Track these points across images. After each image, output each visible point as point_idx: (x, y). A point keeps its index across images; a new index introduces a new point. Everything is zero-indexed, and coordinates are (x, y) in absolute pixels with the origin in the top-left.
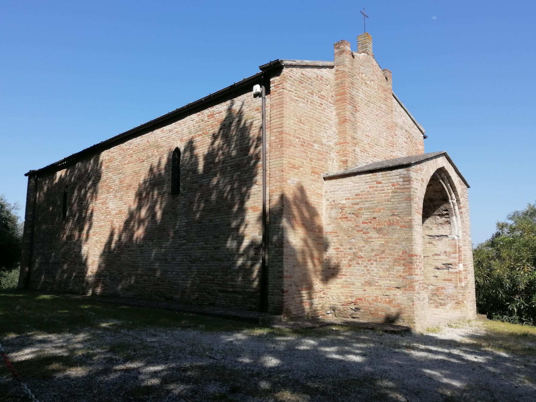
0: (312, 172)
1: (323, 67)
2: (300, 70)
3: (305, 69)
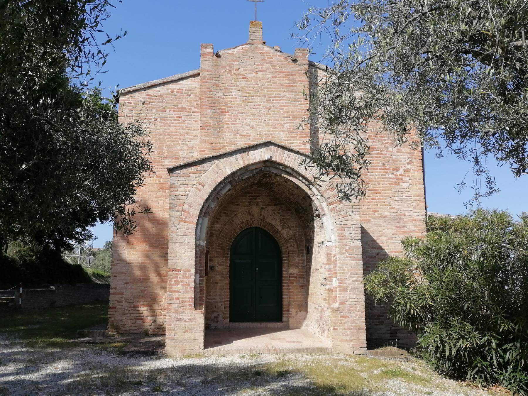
0: (161, 188)
1: (188, 77)
2: (144, 93)
3: (153, 89)
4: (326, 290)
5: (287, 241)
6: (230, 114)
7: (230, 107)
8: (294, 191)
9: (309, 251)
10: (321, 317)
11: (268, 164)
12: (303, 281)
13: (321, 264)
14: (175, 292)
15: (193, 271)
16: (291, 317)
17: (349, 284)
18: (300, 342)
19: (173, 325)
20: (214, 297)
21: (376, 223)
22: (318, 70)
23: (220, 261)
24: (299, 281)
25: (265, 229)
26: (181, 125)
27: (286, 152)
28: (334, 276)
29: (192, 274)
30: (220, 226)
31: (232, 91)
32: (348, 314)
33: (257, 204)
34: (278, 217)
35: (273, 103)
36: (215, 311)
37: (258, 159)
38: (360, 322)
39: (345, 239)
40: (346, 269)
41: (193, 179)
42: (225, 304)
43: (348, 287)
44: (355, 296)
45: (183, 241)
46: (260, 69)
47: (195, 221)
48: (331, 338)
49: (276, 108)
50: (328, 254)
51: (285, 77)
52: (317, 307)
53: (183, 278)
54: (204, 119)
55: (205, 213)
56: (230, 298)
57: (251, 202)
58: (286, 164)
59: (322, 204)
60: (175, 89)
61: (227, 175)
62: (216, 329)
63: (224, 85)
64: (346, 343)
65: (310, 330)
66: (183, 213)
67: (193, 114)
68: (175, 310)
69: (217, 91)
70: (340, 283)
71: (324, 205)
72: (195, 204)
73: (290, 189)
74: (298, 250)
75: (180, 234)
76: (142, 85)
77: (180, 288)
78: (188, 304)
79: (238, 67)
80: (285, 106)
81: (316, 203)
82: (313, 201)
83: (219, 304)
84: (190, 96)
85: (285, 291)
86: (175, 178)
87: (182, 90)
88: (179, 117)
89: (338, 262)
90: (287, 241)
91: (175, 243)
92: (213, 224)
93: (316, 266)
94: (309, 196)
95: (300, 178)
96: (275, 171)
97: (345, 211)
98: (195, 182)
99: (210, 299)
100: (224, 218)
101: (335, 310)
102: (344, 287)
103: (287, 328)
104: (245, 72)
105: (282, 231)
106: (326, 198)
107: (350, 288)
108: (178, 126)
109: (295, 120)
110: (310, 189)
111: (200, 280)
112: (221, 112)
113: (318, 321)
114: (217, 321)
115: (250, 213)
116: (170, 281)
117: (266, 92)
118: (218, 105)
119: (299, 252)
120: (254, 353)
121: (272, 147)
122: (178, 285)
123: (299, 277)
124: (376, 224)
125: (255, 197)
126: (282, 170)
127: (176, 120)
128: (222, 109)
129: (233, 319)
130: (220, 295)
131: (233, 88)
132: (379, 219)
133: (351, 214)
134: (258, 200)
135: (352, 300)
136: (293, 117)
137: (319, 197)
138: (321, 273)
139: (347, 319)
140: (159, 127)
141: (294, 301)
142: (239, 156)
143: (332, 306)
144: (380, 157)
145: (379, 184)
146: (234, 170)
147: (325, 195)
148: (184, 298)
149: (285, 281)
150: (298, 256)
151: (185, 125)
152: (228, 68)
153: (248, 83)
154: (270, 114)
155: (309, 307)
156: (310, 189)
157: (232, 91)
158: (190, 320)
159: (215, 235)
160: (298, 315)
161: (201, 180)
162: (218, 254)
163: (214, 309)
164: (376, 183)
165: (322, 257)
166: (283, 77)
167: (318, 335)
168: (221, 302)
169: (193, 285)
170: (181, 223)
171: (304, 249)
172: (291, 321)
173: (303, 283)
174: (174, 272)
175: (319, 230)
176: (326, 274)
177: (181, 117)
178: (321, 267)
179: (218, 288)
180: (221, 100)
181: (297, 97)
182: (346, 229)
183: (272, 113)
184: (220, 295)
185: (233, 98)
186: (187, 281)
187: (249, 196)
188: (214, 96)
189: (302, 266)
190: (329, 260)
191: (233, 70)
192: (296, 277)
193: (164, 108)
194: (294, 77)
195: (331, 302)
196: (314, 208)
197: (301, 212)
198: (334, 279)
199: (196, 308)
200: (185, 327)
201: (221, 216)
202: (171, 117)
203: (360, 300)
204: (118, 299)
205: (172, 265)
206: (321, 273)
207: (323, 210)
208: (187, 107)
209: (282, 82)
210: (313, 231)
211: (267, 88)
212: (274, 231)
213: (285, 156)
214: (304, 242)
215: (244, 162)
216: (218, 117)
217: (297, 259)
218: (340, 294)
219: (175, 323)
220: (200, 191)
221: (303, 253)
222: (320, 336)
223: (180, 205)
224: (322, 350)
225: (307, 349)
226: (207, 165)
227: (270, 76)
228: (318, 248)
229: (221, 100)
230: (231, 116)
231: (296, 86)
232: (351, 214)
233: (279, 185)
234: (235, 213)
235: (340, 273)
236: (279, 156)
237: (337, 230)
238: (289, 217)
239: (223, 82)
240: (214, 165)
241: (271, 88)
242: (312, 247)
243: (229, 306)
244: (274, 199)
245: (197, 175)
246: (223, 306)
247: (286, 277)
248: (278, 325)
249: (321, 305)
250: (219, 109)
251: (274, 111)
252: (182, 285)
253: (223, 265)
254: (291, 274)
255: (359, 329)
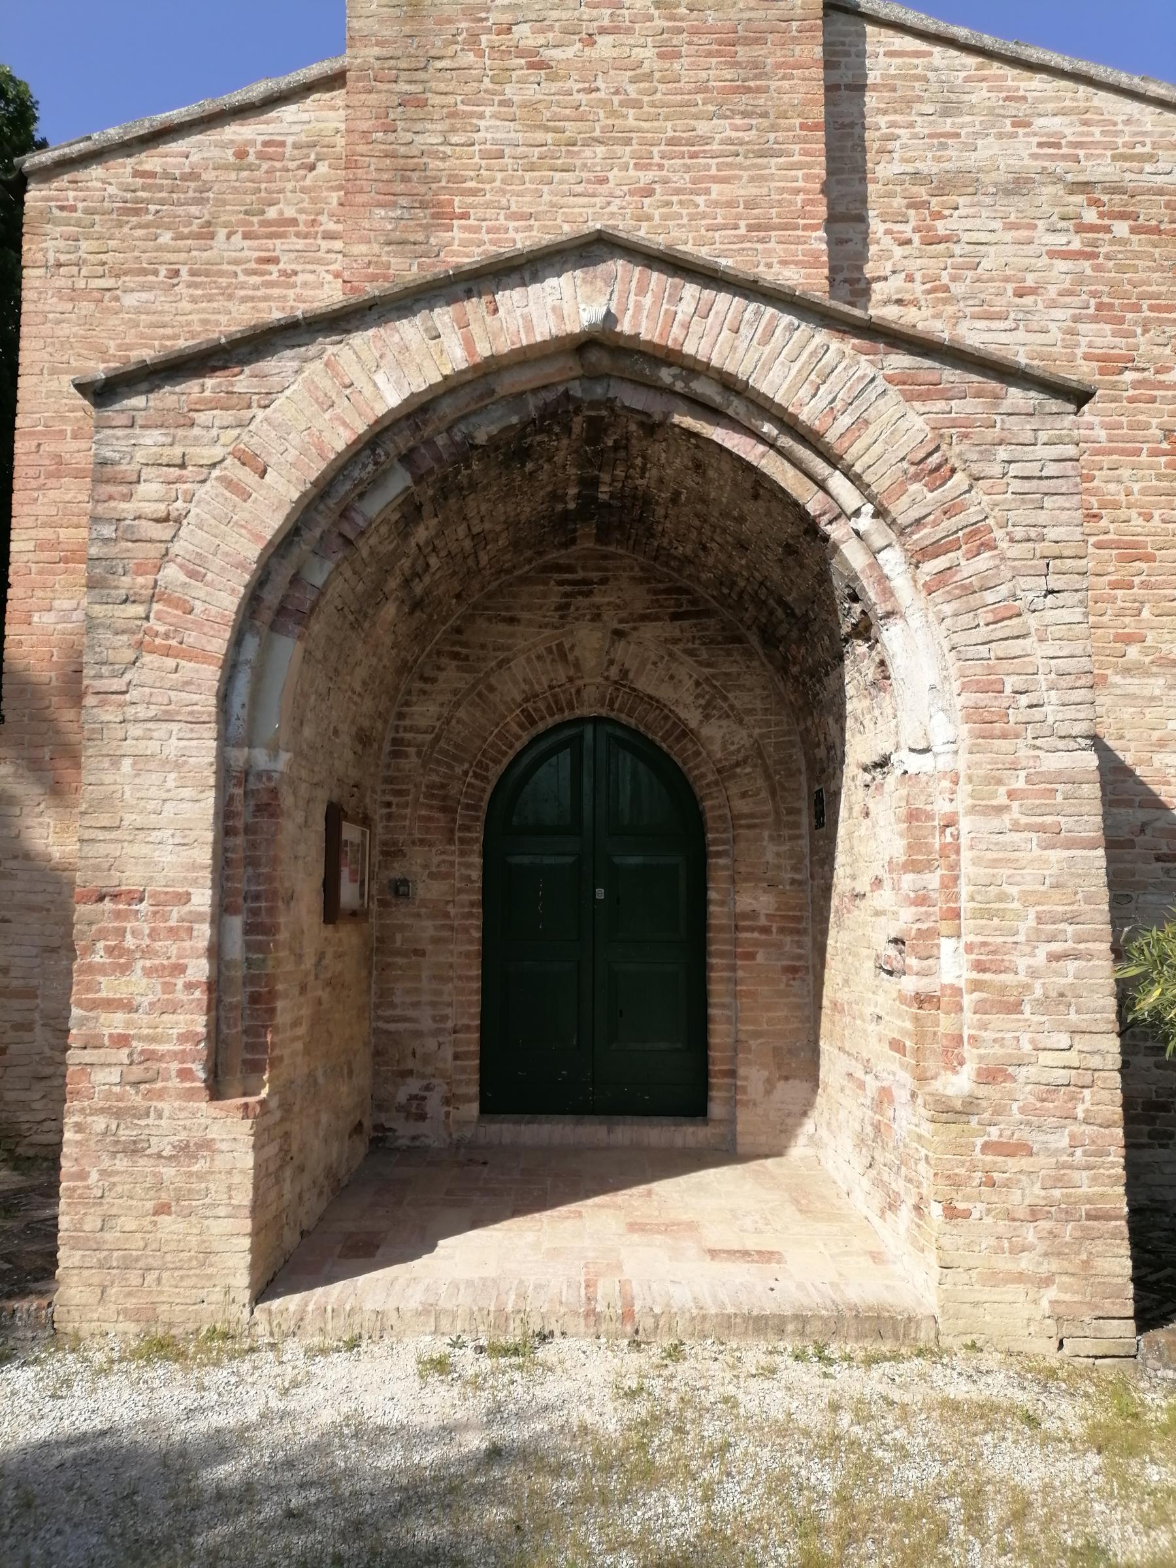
2: (123, 168)
4: (902, 998)
5: (725, 773)
6: (471, 222)
7: (474, 192)
8: (741, 519)
9: (823, 811)
10: (877, 1128)
11: (594, 356)
12: (800, 945)
13: (877, 870)
14: (111, 1005)
15: (203, 899)
16: (746, 1104)
17: (1034, 973)
18: (767, 1256)
19: (94, 1176)
20: (410, 1013)
21: (1132, 690)
22: (870, 29)
23: (436, 860)
24: (779, 945)
25: (632, 722)
26: (276, 292)
27: (691, 291)
28: (945, 927)
29: (197, 917)
30: (433, 709)
31: (482, 123)
32: (1023, 1134)
33: (597, 617)
34: (687, 671)
35: (661, 167)
36: (410, 1073)
37: (544, 329)
38: (1094, 1180)
39: (1004, 736)
40: (1014, 890)
41: (213, 435)
42: (456, 1043)
43: (1027, 987)
44: (1063, 1040)
45: (153, 747)
46: (606, 22)
47: (219, 645)
48: (932, 1258)
49: (678, 191)
50: (913, 816)
51: (719, 54)
52: (859, 1074)
53: (154, 934)
54: (363, 248)
55: (282, 611)
56: (484, 1015)
57: (567, 606)
58: (689, 349)
59: (881, 557)
60: (253, 143)
61: (381, 410)
62: (415, 1152)
63: (450, 100)
64: (1015, 1292)
65: (829, 1166)
66: (156, 607)
67: (325, 245)
68: (108, 1096)
69: (418, 127)
70: (980, 967)
71: (893, 560)
72: (217, 562)
73: (725, 514)
74: (777, 812)
75: (142, 711)
76: (114, 133)
77: (136, 985)
78: (175, 1066)
79: (507, 18)
80: (716, 180)
81: (853, 555)
82: (836, 548)
83: (431, 1044)
84: (312, 168)
85: (718, 989)
86: (120, 433)
87: (282, 144)
88: (268, 261)
89: (966, 855)
90: (725, 773)
91: (115, 760)
92: (407, 704)
93: (853, 877)
94: (810, 528)
95: (767, 428)
96: (633, 398)
97: (1004, 590)
98: (217, 452)
99: (388, 1020)
100: (451, 677)
101: (952, 1113)
102: (1003, 989)
103: (726, 1153)
104: (541, 40)
105: (706, 731)
106: (902, 520)
107: (1039, 992)
108: (266, 298)
109: (761, 241)
110: (822, 485)
111: (249, 946)
112: (435, 216)
113: (861, 1142)
114: (422, 1117)
115: (563, 656)
116: (90, 949)
117: (631, 122)
118: (422, 189)
119: (778, 823)
120: (513, 1337)
121: (618, 266)
122: (125, 969)
123: (782, 930)
124: (1134, 696)
125: (585, 587)
126: (669, 391)
127: (254, 273)
128: (440, 204)
129: (494, 1103)
130: (434, 1004)
131: (488, 111)
132: (1147, 674)
133: (1039, 603)
134: (597, 599)
135: (1046, 1058)
136: (751, 228)
137: (865, 523)
138: (878, 913)
139: (1024, 1162)
140: (186, 305)
141: (757, 1035)
142: (443, 316)
143: (936, 1086)
144: (1153, 400)
145: (1148, 518)
146: (419, 384)
147: (895, 509)
148: (153, 1039)
149: (717, 944)
150: (776, 839)
151: (291, 293)
152: (464, 25)
153: (554, 87)
154: (649, 218)
155: (824, 1061)
156: (822, 485)
157: (482, 123)
158: (186, 1151)
159: (412, 750)
160: (777, 1095)
161: (250, 441)
162: (428, 830)
163: (410, 1064)
164: (1133, 513)
165: (883, 835)
166: (710, 54)
167: (866, 1212)
168: (437, 1032)
169: (200, 969)
170: (147, 658)
171: (804, 805)
172: (746, 1120)
173: (800, 957)
174: (108, 905)
175: (866, 703)
176: (904, 920)
177: (275, 261)
178: (878, 882)
179: (425, 974)
180: (434, 164)
181: (772, 136)
182: (1011, 683)
183: (657, 214)
184: (434, 1004)
185: (486, 155)
186: (174, 950)
187: (561, 583)
188: (402, 150)
189: (793, 882)
190: (916, 845)
191: (489, 31)
192: (765, 930)
193: (209, 224)
194: (757, 51)
195: (931, 1065)
196: (839, 586)
197: (787, 624)
198: (947, 945)
199: (216, 1090)
200: (159, 1185)
201: (439, 668)
202: (236, 262)
203: (1095, 1062)
204: (17, 1017)
205: (97, 868)
206: (878, 913)
207: (888, 593)
208: (302, 218)
209: (704, 75)
210: (841, 718)
211: (637, 104)
212: (668, 734)
213: (685, 308)
214: (803, 778)
215: (469, 344)
216: (420, 237)
217: (770, 852)
218: (984, 1026)
219: (106, 1163)
220: (246, 496)
221: (796, 825)
222: (876, 1221)
223: (140, 571)
224: (883, 1331)
225: (802, 1320)
226: (279, 364)
227: (649, 53)
228: (861, 792)
229: (434, 164)
230: (477, 230)
231: (766, 90)
232: (1039, 603)
233: (675, 499)
234: (502, 655)
235: (979, 914)
236: (651, 310)
237: (964, 688)
238: (734, 669)
239: (442, 87)
240: (318, 365)
241: (653, 105)
242: (837, 794)
243: (475, 1048)
244: (667, 591)
245: (228, 417)
246: (448, 1052)
247: (722, 929)
248: (689, 1134)
249: (879, 1067)
250: (423, 206)
251: (669, 204)
252: (148, 972)
253: (448, 876)
254: (745, 916)
255: (1089, 1217)
